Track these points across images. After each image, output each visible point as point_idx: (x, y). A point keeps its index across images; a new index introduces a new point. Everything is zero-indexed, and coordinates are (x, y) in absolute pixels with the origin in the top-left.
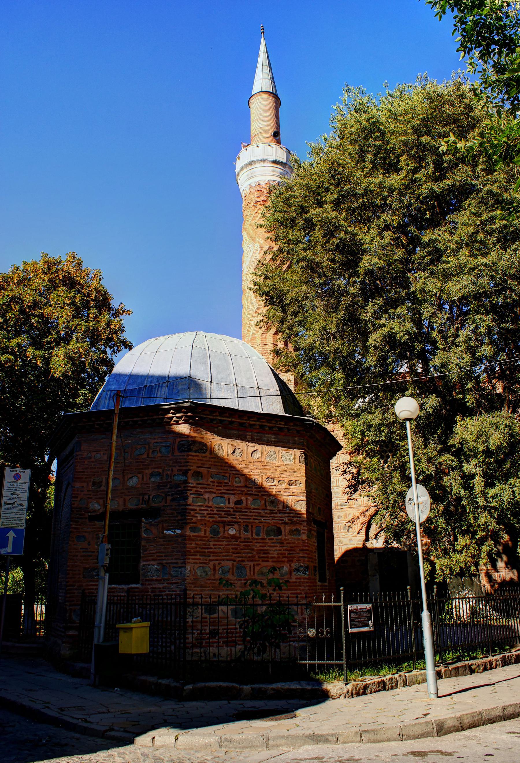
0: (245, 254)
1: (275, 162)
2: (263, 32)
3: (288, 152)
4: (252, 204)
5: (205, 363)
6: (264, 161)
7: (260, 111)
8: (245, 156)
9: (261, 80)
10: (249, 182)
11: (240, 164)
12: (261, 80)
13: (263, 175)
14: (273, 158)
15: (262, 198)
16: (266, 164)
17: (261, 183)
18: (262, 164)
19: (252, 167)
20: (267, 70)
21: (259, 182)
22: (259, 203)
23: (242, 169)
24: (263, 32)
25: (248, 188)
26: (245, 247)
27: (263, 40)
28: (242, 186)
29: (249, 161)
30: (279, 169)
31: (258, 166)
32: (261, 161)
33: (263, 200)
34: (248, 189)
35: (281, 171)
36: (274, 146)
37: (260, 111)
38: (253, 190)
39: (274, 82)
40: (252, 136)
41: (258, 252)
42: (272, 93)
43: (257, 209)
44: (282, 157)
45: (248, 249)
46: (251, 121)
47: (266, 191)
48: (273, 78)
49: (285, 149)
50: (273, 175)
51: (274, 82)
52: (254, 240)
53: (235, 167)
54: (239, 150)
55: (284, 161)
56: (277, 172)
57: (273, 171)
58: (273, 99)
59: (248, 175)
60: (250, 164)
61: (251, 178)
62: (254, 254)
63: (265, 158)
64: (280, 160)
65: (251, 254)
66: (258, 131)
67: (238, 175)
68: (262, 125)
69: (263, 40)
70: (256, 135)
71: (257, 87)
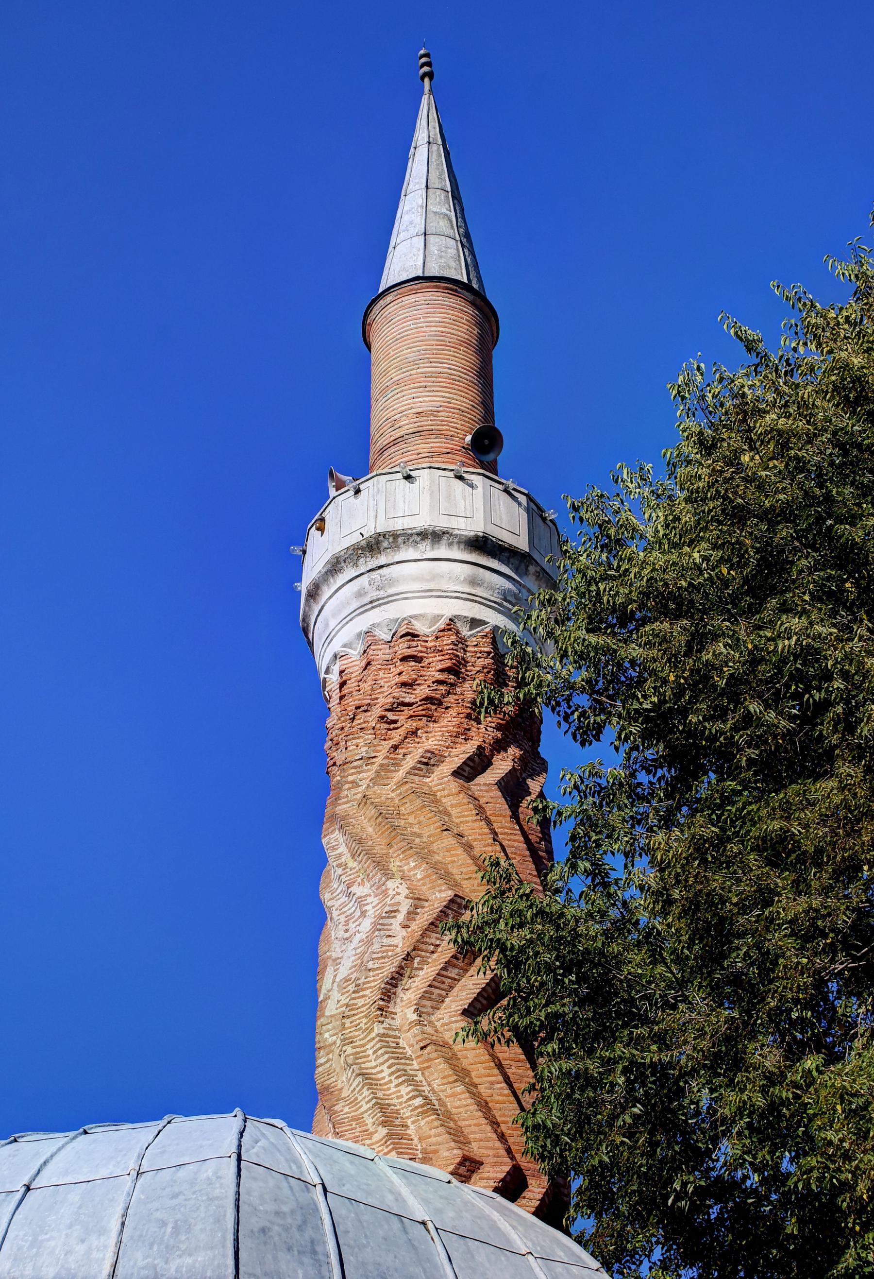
0: (334, 931)
1: (482, 544)
2: (430, 75)
3: (535, 512)
4: (377, 711)
5: (313, 1249)
6: (435, 536)
7: (415, 359)
8: (351, 516)
9: (420, 236)
10: (362, 623)
11: (320, 549)
12: (420, 236)
13: (428, 593)
14: (475, 527)
15: (422, 691)
16: (442, 551)
17: (421, 628)
18: (426, 550)
19: (382, 560)
20: (442, 205)
21: (408, 620)
22: (408, 712)
23: (335, 567)
24: (430, 75)
25: (360, 647)
26: (332, 896)
27: (426, 102)
28: (329, 639)
29: (369, 531)
30: (496, 580)
31: (402, 557)
32: (423, 535)
33: (428, 699)
34: (355, 653)
35: (508, 585)
36: (477, 480)
37: (415, 359)
38: (382, 653)
39: (472, 253)
40: (374, 449)
41: (401, 917)
42: (467, 287)
43: (396, 736)
44: (510, 524)
45: (351, 907)
46: (374, 392)
47: (435, 665)
48: (467, 235)
49: (523, 499)
50: (471, 598)
51: (472, 253)
52: (381, 865)
53: (297, 565)
54: (322, 500)
55: (522, 543)
56: (492, 588)
57: (473, 582)
58: (470, 310)
59: (360, 594)
60: (373, 545)
61: (374, 604)
62: (380, 925)
63: (442, 523)
64: (508, 539)
65: (366, 925)
66: (407, 425)
67: (313, 594)
68: (425, 401)
69: (426, 102)
70: (395, 442)
71: (404, 258)
